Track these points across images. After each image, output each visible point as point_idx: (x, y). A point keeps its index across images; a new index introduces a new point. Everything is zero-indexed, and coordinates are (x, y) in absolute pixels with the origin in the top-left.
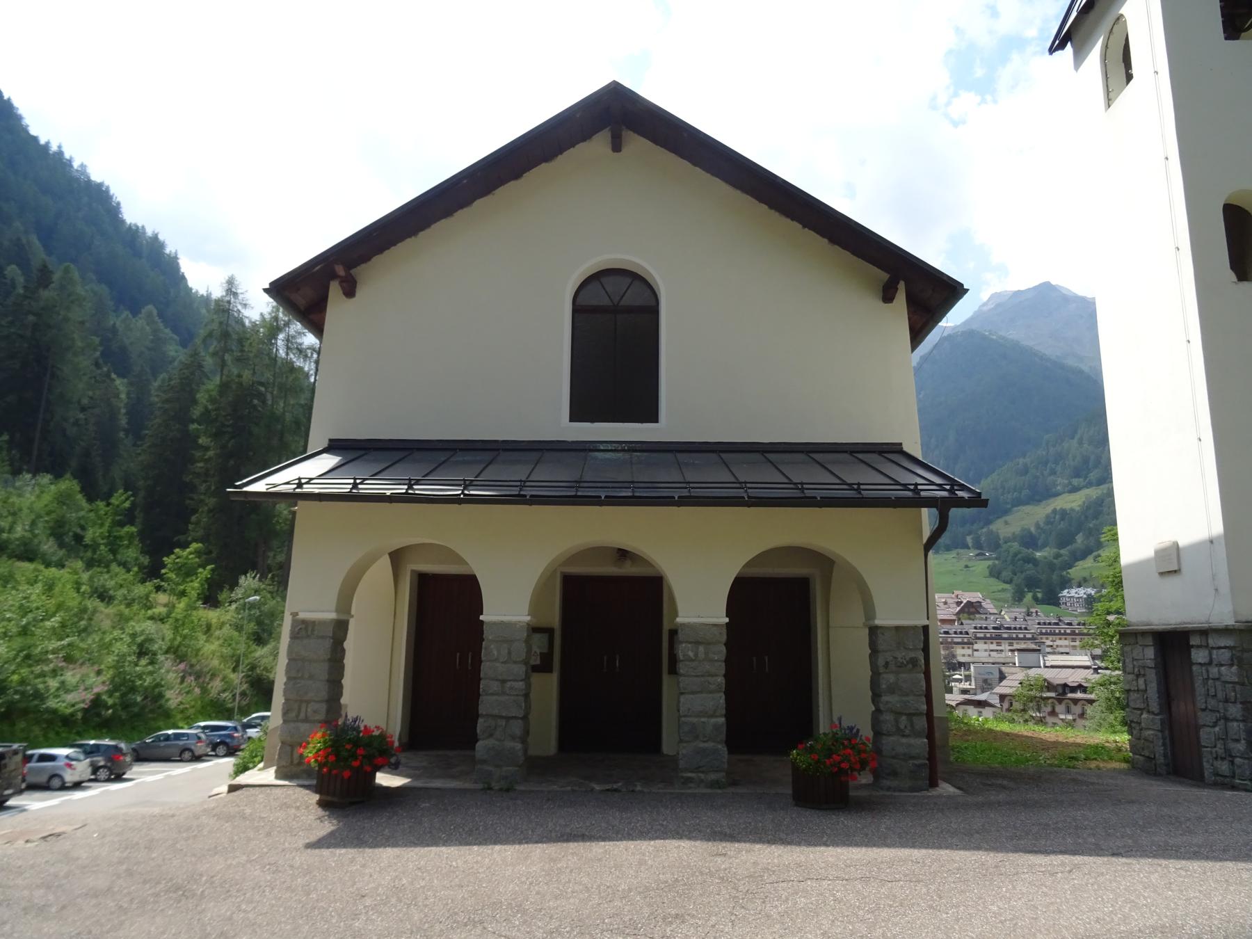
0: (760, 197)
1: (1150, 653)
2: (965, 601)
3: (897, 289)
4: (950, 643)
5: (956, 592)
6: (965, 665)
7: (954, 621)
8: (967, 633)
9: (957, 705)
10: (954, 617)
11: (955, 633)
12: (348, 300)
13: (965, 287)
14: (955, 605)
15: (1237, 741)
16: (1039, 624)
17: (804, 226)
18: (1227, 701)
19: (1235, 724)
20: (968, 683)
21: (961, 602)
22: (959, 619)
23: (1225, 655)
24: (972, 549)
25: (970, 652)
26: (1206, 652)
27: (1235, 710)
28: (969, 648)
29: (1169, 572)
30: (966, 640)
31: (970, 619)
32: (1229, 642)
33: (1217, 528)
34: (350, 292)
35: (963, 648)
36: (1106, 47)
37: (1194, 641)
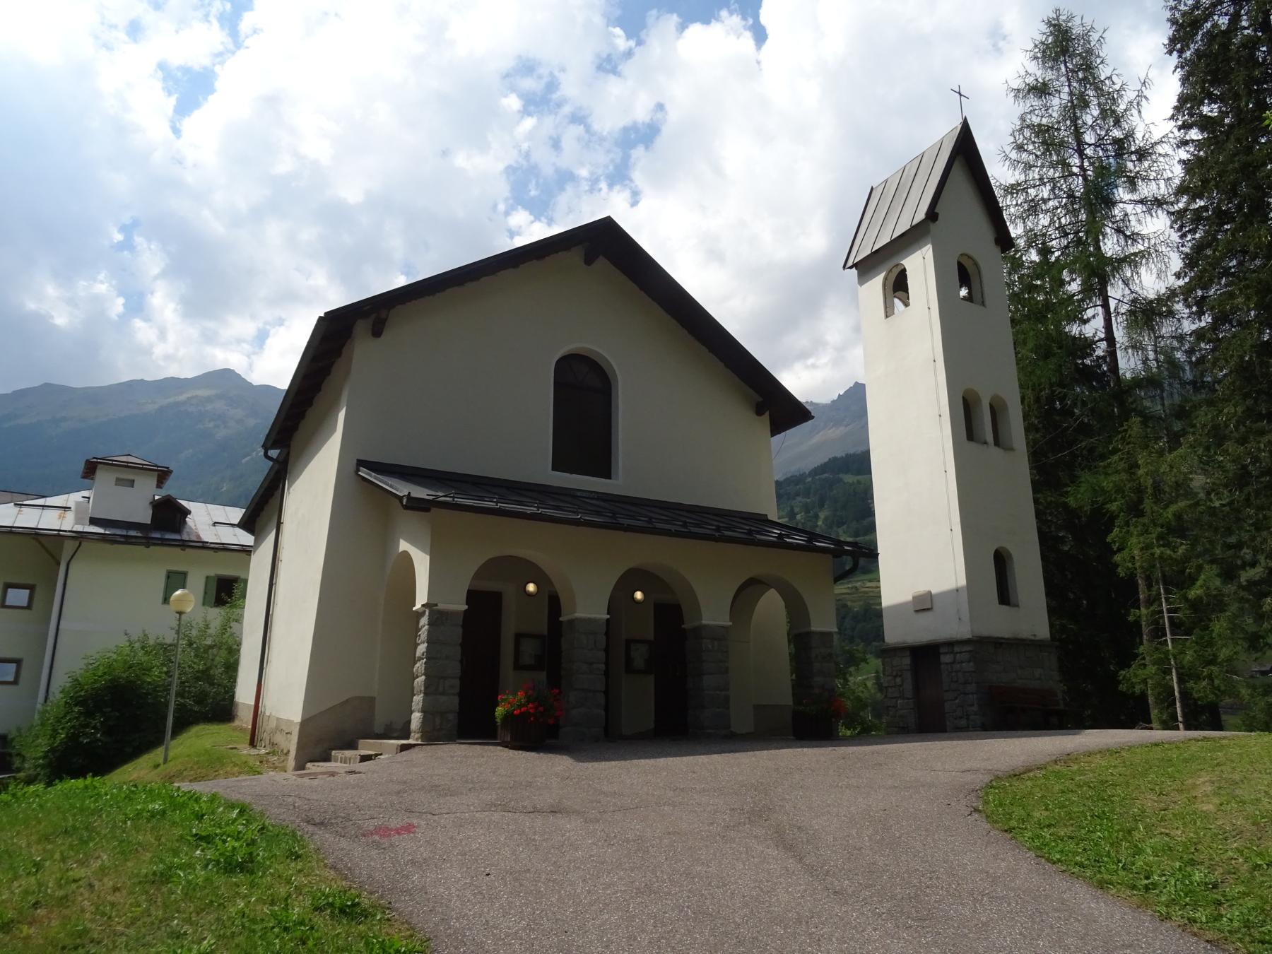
15: (973, 705)
17: (710, 351)
19: (971, 696)
26: (952, 655)
29: (924, 610)
33: (962, 581)
34: (377, 332)
36: (885, 279)
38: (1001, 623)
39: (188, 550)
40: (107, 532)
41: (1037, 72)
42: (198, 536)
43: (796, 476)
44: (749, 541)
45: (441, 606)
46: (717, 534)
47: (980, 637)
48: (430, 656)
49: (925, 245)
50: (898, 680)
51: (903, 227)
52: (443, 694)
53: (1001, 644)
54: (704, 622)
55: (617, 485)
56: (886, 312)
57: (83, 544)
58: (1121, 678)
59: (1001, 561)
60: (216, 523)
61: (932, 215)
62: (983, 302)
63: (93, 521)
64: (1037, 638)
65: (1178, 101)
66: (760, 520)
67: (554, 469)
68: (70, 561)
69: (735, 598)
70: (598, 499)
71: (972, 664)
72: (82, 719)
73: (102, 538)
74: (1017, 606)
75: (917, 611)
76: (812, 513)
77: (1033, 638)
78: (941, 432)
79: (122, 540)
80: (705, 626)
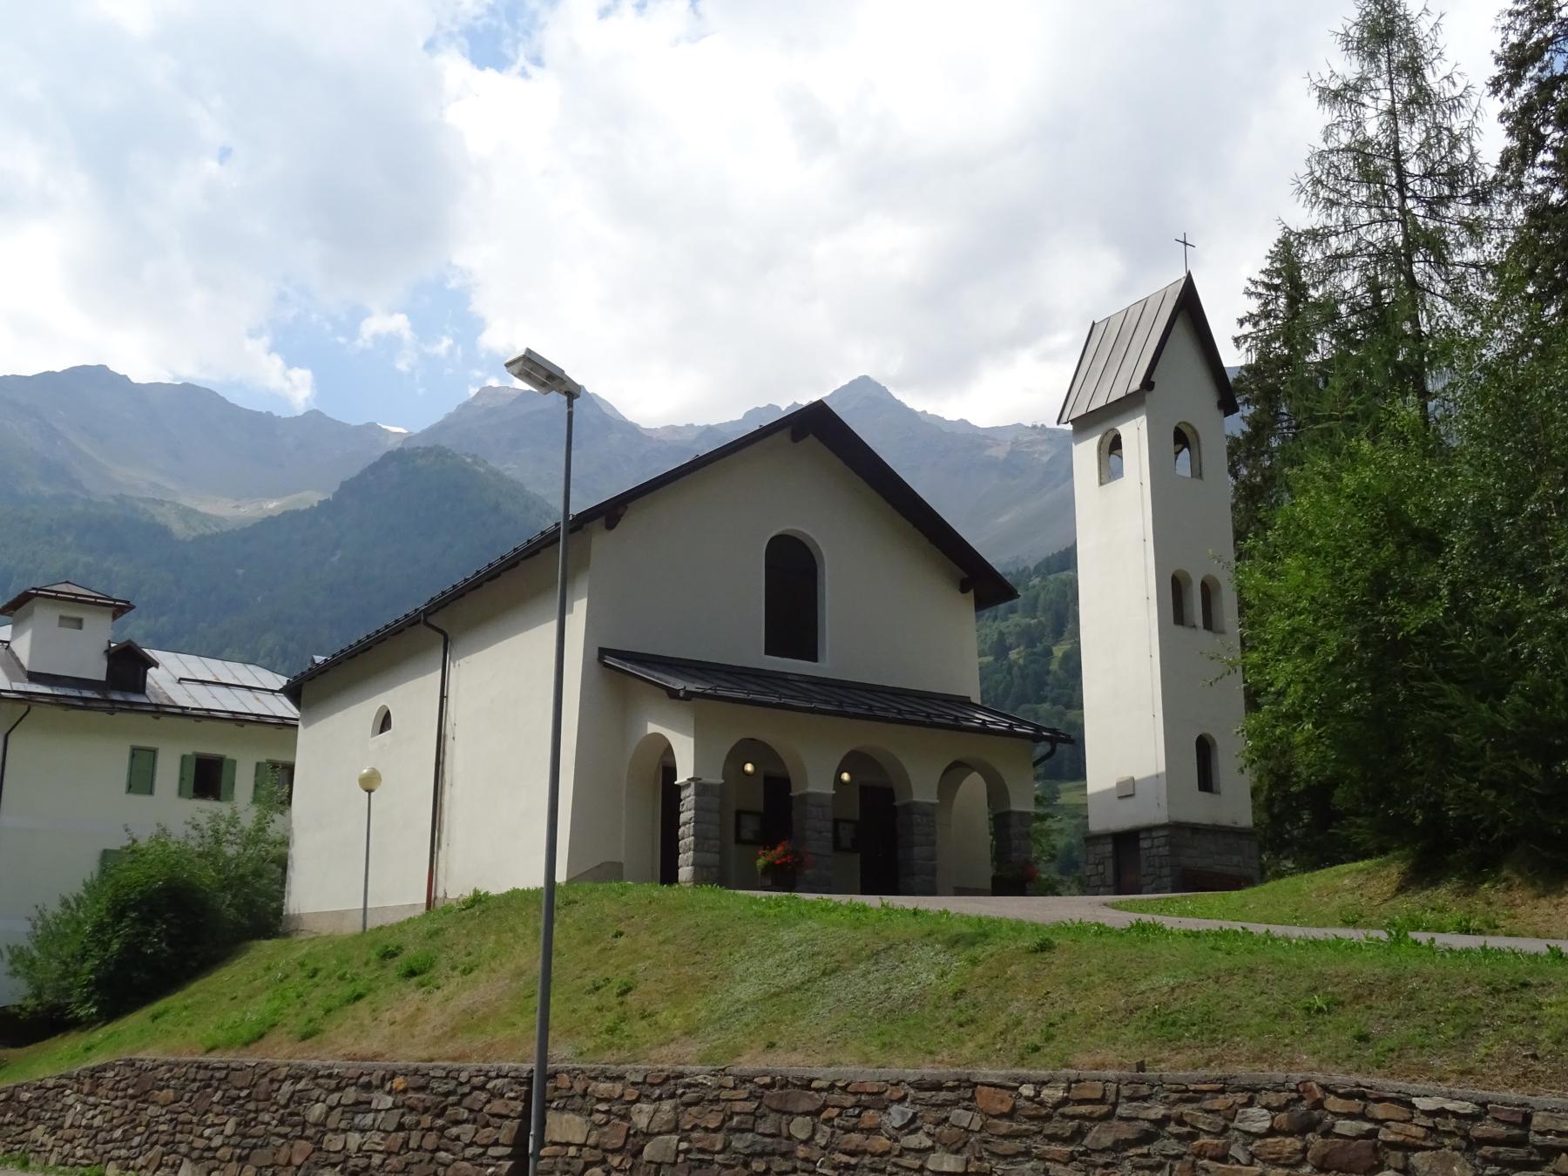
0: (889, 498)
1: (1109, 848)
27: (1166, 871)
32: (1165, 833)
33: (1162, 768)
36: (1101, 442)
38: (1200, 809)
39: (164, 719)
40: (56, 693)
41: (1349, 68)
42: (169, 698)
44: (956, 727)
45: (705, 780)
46: (928, 720)
48: (697, 820)
49: (1140, 416)
50: (1101, 868)
51: (1119, 393)
52: (707, 851)
53: (1197, 829)
54: (915, 799)
55: (827, 666)
56: (1100, 478)
57: (32, 708)
59: (1205, 749)
60: (181, 679)
61: (1148, 384)
62: (1201, 475)
63: (34, 677)
65: (1501, 161)
66: (962, 703)
67: (767, 652)
68: (10, 732)
69: (943, 774)
70: (807, 682)
71: (1167, 848)
72: (138, 926)
73: (57, 701)
74: (1219, 793)
75: (1120, 798)
76: (1039, 648)
78: (1148, 614)
79: (81, 704)
80: (916, 803)
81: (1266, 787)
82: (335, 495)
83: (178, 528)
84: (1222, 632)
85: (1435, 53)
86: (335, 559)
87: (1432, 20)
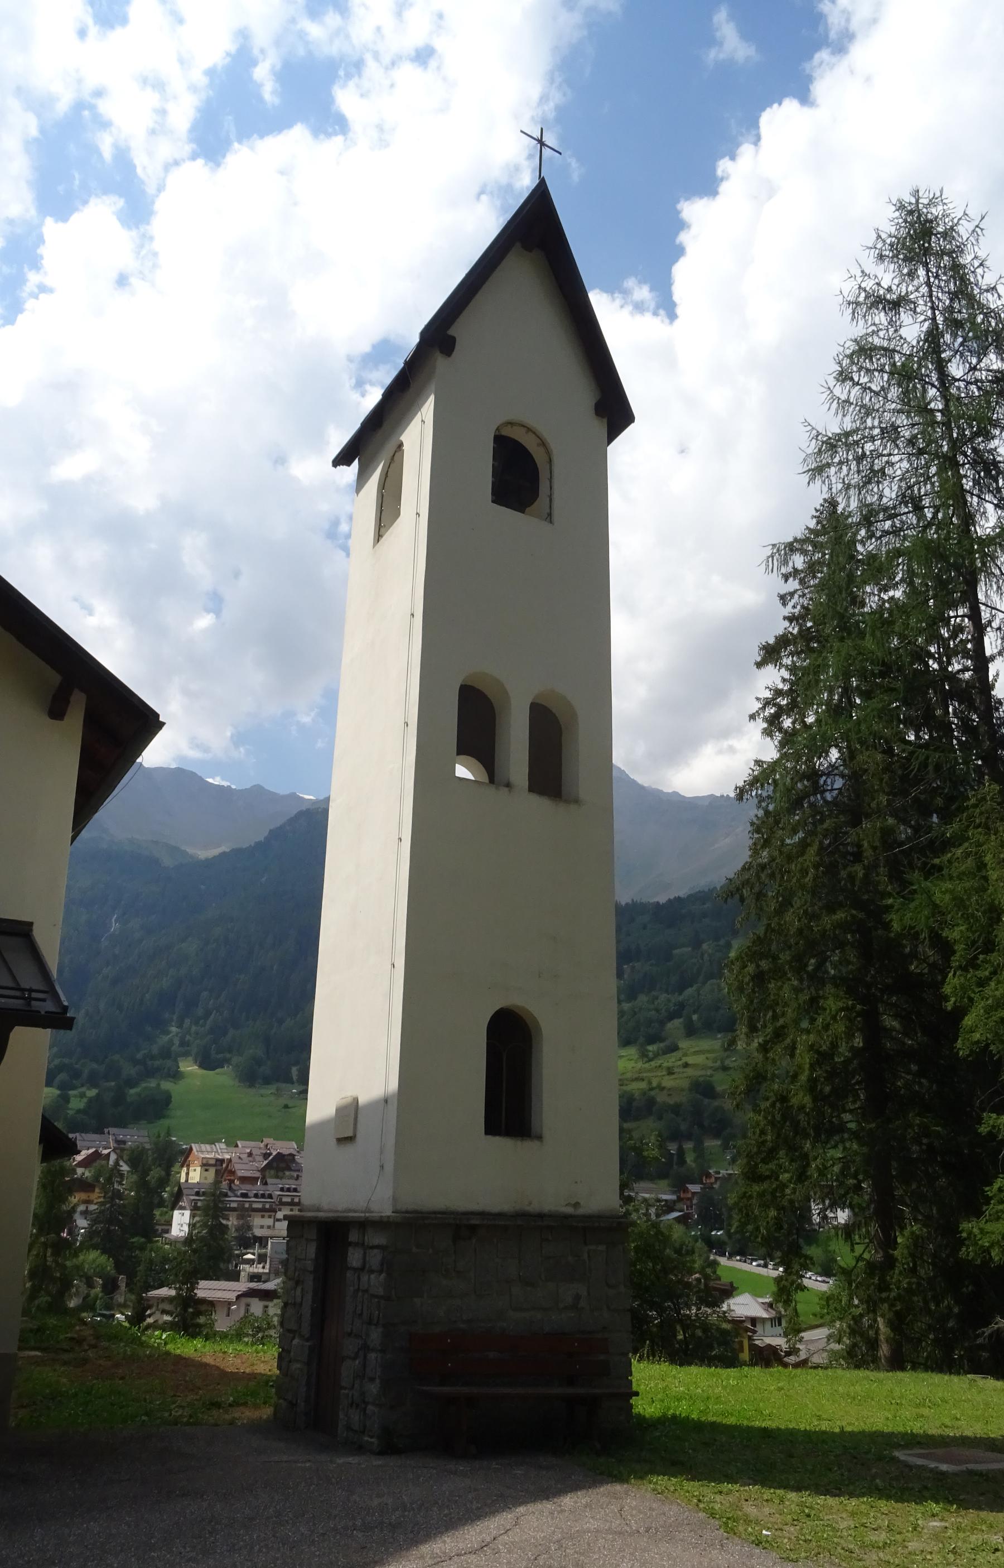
2: (274, 1153)
3: (69, 702)
4: (247, 1210)
5: (266, 1140)
6: (262, 1241)
7: (257, 1179)
8: (270, 1196)
9: (238, 1297)
10: (258, 1174)
11: (256, 1196)
12: (48, 718)
13: (161, 719)
14: (261, 1158)
16: (282, 1190)
18: (370, 1323)
20: (261, 1265)
21: (270, 1154)
22: (264, 1178)
23: (375, 1258)
24: (296, 1084)
25: (269, 1222)
27: (375, 1336)
28: (270, 1217)
30: (267, 1206)
31: (277, 1177)
33: (394, 1085)
35: (263, 1217)
37: (353, 1236)
43: (704, 891)
47: (416, 1212)
53: (473, 1228)
58: (964, 1235)
62: (550, 515)
64: (581, 1211)
74: (540, 1138)
76: (722, 942)
77: (570, 1210)
81: (807, 1066)
82: (265, 838)
83: (167, 862)
84: (577, 801)
85: (976, 263)
86: (264, 879)
87: (971, 227)
